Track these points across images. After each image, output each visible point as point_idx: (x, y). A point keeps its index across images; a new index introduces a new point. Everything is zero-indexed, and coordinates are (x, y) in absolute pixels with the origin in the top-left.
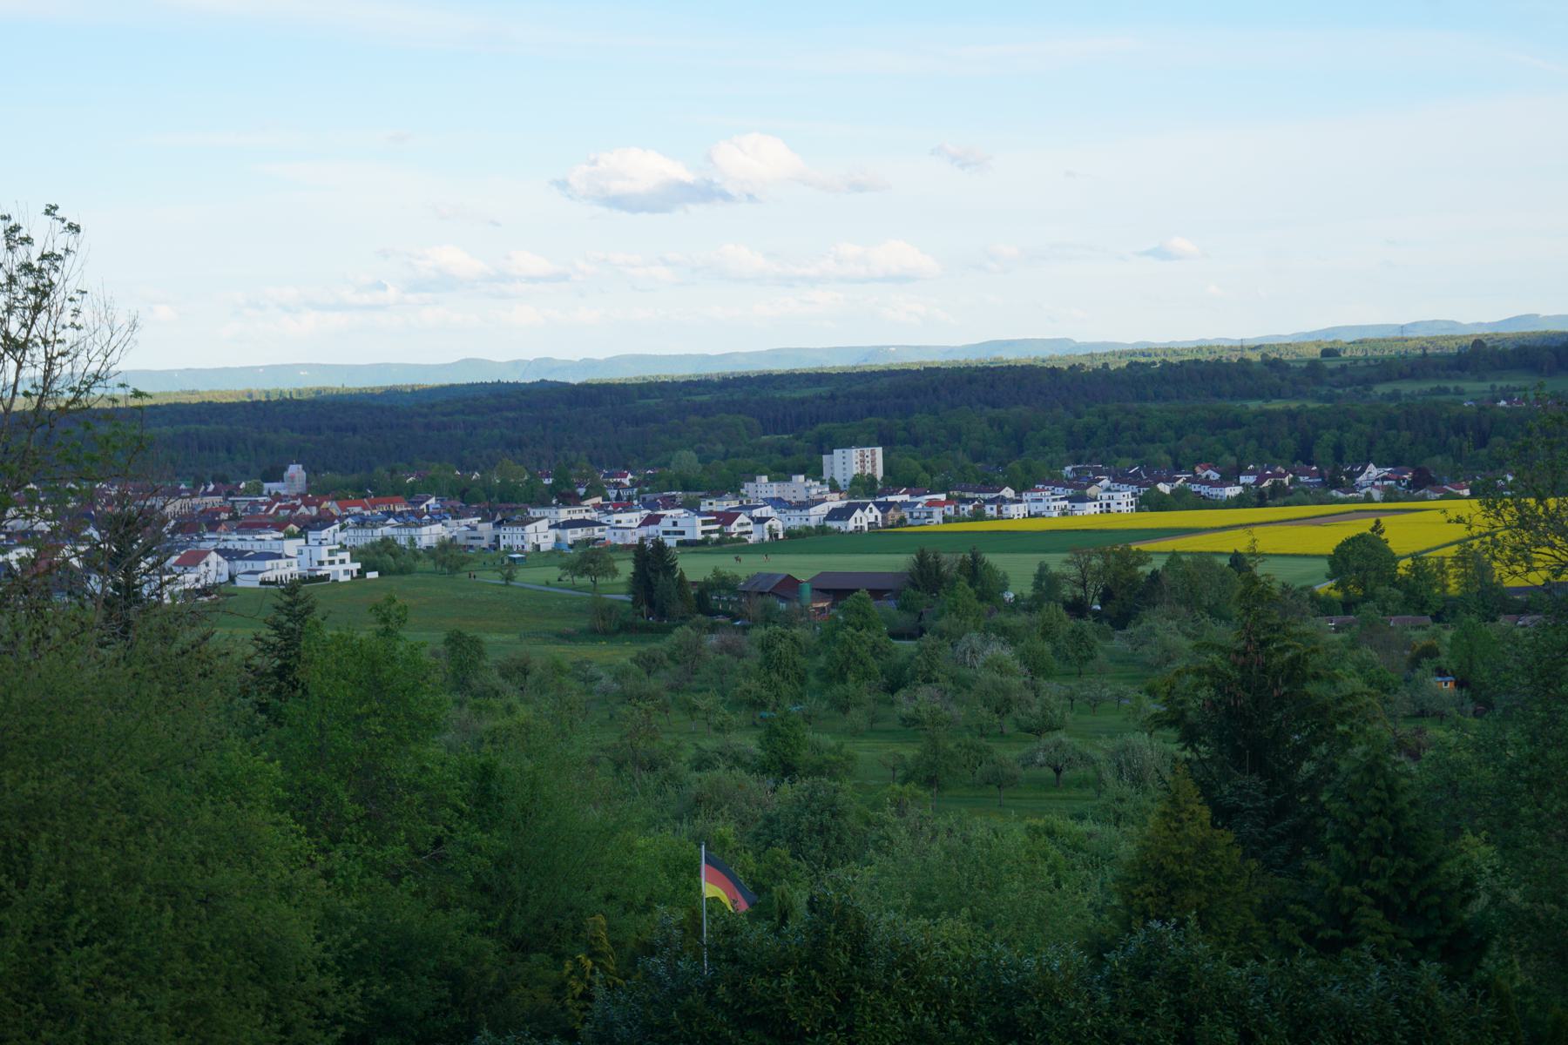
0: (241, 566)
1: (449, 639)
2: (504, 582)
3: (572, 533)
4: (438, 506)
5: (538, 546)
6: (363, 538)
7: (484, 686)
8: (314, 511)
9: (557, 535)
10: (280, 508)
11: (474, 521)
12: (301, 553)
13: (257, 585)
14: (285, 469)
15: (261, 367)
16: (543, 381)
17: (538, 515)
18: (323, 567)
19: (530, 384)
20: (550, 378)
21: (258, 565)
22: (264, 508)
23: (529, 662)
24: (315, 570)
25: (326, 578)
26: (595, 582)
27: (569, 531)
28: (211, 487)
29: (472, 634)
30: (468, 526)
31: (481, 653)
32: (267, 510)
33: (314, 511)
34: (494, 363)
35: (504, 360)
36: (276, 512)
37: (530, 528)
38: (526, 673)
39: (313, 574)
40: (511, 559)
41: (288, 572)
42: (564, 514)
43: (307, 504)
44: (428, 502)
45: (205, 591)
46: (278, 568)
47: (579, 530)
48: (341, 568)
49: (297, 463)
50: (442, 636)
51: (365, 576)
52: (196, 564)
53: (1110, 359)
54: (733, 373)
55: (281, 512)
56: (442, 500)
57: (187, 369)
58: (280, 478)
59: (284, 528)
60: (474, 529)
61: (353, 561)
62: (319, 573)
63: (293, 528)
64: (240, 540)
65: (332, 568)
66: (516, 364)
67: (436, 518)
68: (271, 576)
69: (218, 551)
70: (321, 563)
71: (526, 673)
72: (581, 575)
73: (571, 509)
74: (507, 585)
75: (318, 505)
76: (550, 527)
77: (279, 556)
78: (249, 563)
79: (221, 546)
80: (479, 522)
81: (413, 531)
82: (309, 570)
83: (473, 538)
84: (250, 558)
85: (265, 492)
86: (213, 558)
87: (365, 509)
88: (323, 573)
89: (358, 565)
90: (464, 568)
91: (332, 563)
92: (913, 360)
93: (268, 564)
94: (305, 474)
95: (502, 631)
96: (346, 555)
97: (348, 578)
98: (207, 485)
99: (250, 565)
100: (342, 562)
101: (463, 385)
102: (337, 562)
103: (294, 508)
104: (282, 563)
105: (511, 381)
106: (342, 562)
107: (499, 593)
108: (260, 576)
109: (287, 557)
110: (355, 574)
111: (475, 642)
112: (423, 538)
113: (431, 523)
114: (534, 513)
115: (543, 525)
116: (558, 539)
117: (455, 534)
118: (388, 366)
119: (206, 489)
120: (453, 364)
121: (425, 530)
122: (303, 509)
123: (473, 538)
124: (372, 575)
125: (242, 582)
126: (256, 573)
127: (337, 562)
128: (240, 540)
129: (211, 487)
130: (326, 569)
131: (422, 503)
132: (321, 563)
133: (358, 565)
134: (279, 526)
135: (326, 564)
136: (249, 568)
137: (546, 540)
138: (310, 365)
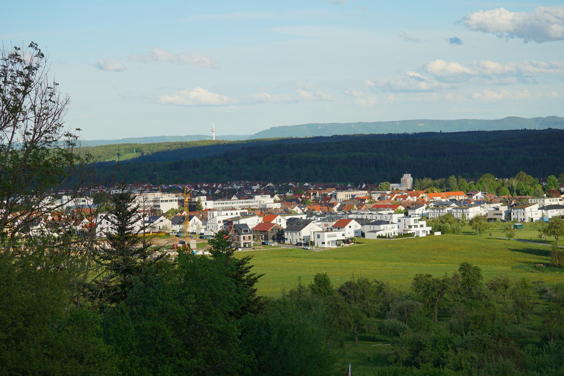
0: (367, 228)
1: (461, 268)
2: (507, 238)
3: (551, 212)
4: (483, 197)
5: (532, 219)
6: (434, 214)
7: (480, 293)
8: (415, 199)
9: (543, 213)
10: (397, 197)
11: (498, 205)
12: (399, 221)
13: (376, 238)
14: (402, 176)
15: (398, 121)
16: (550, 129)
17: (533, 202)
18: (411, 229)
19: (543, 130)
20: (554, 127)
21: (376, 227)
22: (389, 197)
23: (509, 281)
24: (407, 231)
25: (412, 235)
26: (557, 239)
27: (549, 211)
28: (364, 186)
29: (475, 266)
30: (494, 208)
31: (479, 276)
32: (391, 198)
33: (415, 199)
34: (524, 119)
35: (530, 118)
36: (396, 199)
37: (527, 209)
38: (506, 287)
39: (406, 233)
40: (515, 225)
41: (392, 231)
42: (548, 202)
43: (412, 196)
44: (477, 195)
45: (347, 241)
46: (387, 229)
47: (555, 210)
48: (421, 229)
49: (408, 173)
50: (458, 267)
51: (434, 234)
52: (343, 227)
53: (198, 143)
54: (223, 140)
55: (398, 199)
56: (485, 194)
57: (359, 123)
58: (399, 182)
59: (396, 208)
60: (497, 209)
61: (428, 225)
62: (409, 232)
63: (402, 208)
64: (370, 214)
65: (416, 229)
66: (536, 120)
67: (479, 203)
68: (383, 233)
69: (357, 220)
70: (410, 227)
71: (506, 287)
72: (550, 235)
73: (551, 199)
74: (509, 239)
75: (418, 196)
76: (539, 209)
77: (388, 223)
78: (372, 226)
79: (360, 217)
80: (502, 205)
81: (464, 210)
82: (404, 230)
83: (497, 214)
84: (373, 224)
85: (391, 189)
86: (353, 223)
87: (443, 198)
88: (411, 232)
89: (430, 228)
90: (487, 231)
91: (416, 226)
92: (232, 140)
93: (382, 227)
94: (412, 178)
95: (503, 265)
96: (424, 223)
97: (425, 235)
98: (362, 185)
99: (372, 228)
100: (422, 226)
101: (399, 135)
102: (419, 226)
103: (405, 197)
104: (389, 226)
105: (491, 131)
106: (422, 226)
107: (505, 244)
108: (378, 234)
109: (392, 223)
110: (429, 233)
111: (477, 269)
112: (470, 214)
113: (475, 206)
114: (531, 201)
115: (536, 206)
116: (543, 215)
117: (487, 212)
118: (317, 125)
119: (361, 186)
120: (502, 119)
121: (471, 210)
122: (409, 198)
123: (497, 214)
124: (438, 233)
125: (368, 236)
126: (375, 232)
127: (419, 226)
128: (370, 214)
129: (364, 186)
130: (413, 230)
131: (474, 195)
132: (410, 227)
133: (430, 228)
134: (394, 207)
135: (413, 227)
136: (372, 229)
137: (536, 216)
138: (425, 120)
